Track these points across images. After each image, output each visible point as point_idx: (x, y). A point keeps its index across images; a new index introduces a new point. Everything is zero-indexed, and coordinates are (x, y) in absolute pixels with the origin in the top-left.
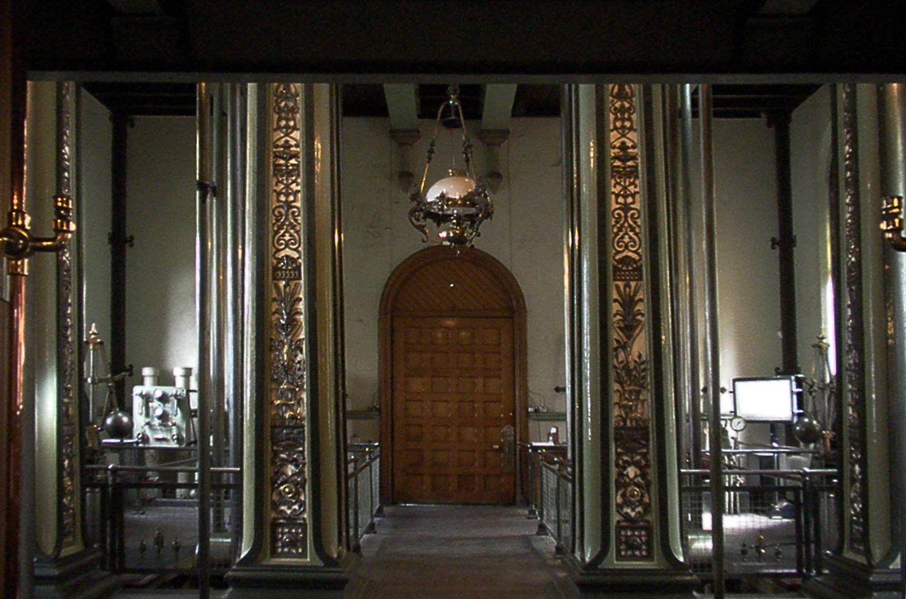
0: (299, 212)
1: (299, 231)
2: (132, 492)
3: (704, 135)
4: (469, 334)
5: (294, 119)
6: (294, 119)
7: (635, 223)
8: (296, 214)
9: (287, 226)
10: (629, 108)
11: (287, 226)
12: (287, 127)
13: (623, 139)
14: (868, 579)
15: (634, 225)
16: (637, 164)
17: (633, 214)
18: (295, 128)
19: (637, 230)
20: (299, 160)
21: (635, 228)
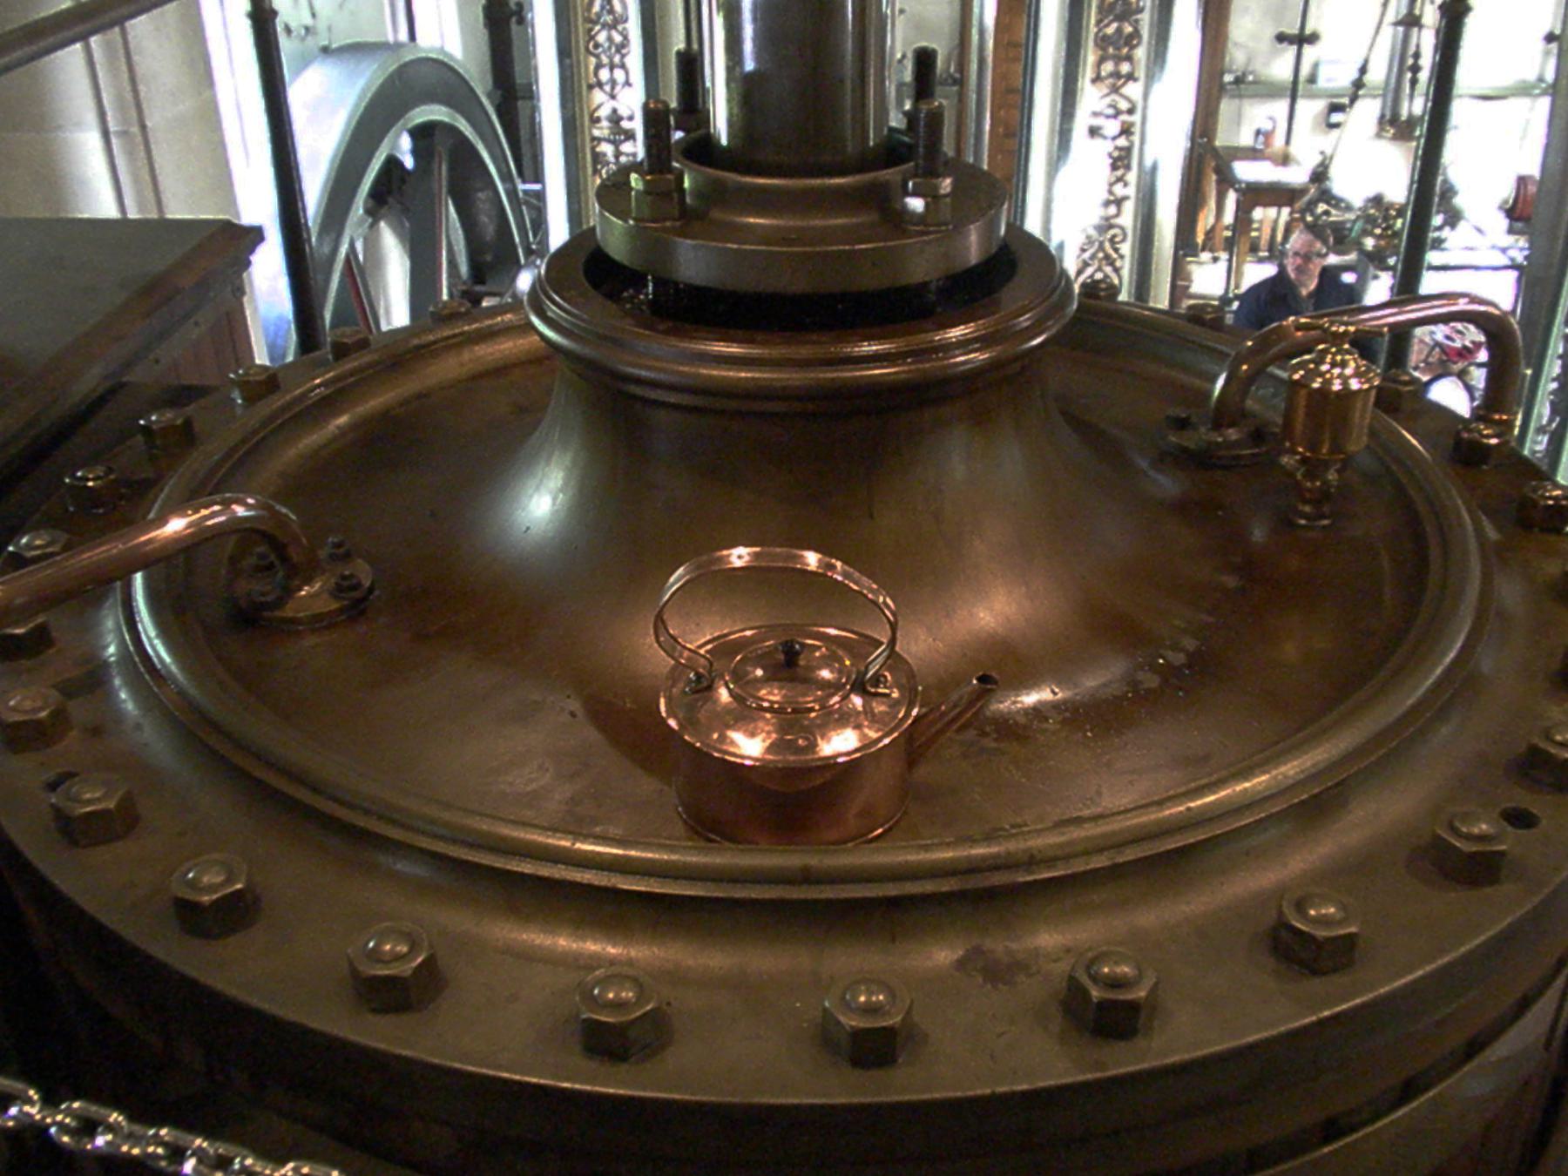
0: (1125, 235)
1: (1121, 268)
2: (370, 220)
3: (869, 115)
4: (488, 238)
5: (1129, 58)
6: (1129, 58)
7: (1116, 250)
8: (1117, 239)
9: (1100, 260)
10: (1131, 36)
11: (1100, 260)
12: (1116, 75)
13: (1114, 97)
14: (764, 672)
15: (1115, 256)
16: (1132, 144)
17: (1114, 236)
18: (1131, 77)
19: (1118, 264)
20: (1132, 138)
21: (1115, 260)
